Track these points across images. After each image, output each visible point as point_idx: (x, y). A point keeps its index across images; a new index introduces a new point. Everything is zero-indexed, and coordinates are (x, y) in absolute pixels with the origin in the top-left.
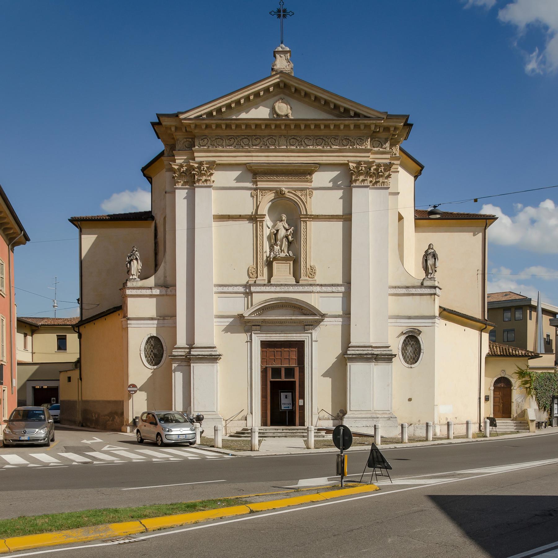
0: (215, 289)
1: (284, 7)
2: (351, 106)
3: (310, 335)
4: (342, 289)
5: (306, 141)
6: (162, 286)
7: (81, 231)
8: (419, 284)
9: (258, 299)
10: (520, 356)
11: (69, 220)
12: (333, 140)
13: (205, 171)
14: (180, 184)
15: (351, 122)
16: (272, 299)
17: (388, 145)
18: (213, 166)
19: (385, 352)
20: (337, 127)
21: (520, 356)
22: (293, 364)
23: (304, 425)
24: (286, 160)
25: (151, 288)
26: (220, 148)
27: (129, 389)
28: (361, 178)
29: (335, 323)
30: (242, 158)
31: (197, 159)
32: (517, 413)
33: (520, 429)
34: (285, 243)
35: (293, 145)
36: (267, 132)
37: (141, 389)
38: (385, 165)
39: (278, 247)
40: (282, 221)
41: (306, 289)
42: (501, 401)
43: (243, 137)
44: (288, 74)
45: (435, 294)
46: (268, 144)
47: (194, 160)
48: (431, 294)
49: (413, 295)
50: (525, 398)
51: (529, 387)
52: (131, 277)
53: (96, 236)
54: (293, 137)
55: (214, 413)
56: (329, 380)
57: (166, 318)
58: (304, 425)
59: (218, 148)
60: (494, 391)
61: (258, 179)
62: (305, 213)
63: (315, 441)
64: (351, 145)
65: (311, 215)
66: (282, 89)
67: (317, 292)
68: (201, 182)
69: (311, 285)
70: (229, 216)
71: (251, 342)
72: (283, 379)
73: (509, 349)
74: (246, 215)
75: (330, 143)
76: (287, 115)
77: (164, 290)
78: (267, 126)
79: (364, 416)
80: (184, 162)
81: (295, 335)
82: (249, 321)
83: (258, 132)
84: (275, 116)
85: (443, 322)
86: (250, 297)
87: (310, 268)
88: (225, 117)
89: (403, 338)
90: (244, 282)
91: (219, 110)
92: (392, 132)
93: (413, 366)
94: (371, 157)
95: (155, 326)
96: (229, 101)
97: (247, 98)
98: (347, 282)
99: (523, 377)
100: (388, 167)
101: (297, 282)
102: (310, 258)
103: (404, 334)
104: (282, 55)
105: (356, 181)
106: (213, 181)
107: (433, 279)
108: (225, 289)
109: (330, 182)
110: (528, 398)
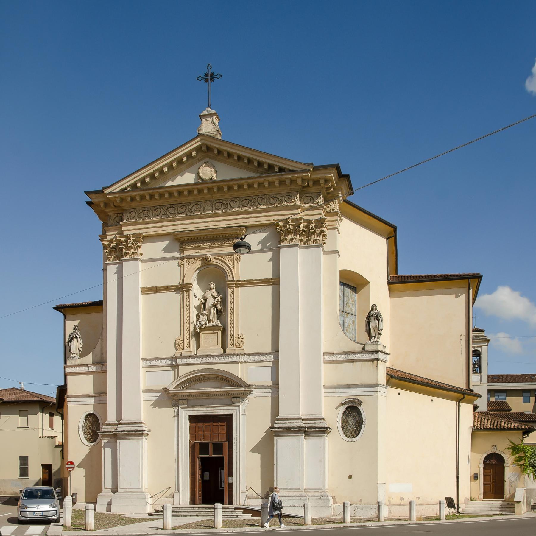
0: (142, 363)
1: (212, 71)
2: (275, 161)
3: (237, 408)
4: (271, 357)
5: (232, 203)
6: (97, 363)
7: (65, 318)
8: (361, 349)
9: (183, 371)
10: (511, 429)
11: (54, 308)
12: (259, 200)
13: (132, 244)
14: (111, 260)
15: (275, 178)
16: (201, 371)
17: (321, 200)
18: (140, 239)
19: (316, 425)
20: (260, 185)
21: (511, 429)
22: (222, 439)
23: (232, 504)
24: (211, 225)
25: (87, 365)
26: (147, 220)
27: (68, 466)
28: (290, 237)
29: (263, 395)
30: (168, 227)
31: (125, 233)
32: (510, 493)
33: (505, 511)
34: (213, 312)
35: (219, 209)
36: (191, 199)
37: (79, 466)
38: (316, 221)
39: (205, 317)
40: (210, 289)
41: (233, 359)
42: (493, 480)
43: (169, 206)
44: (213, 138)
45: (377, 360)
46: (193, 211)
47: (123, 234)
48: (373, 360)
49: (353, 361)
50: (519, 477)
51: (523, 464)
52: (71, 356)
53: (79, 321)
54: (218, 201)
55: (139, 490)
56: (257, 456)
57: (102, 395)
58: (232, 504)
59: (145, 220)
60: (484, 468)
61: (184, 248)
62: (232, 279)
63: (223, 521)
64: (278, 204)
65: (237, 281)
66: (206, 152)
67: (245, 362)
68: (128, 255)
69: (237, 355)
70: (156, 287)
71: (178, 417)
72: (211, 455)
73: (501, 422)
74: (173, 286)
75: (257, 203)
76: (211, 179)
77: (100, 366)
78: (190, 192)
79: (291, 494)
80: (114, 238)
81: (222, 408)
82: (174, 396)
83: (183, 200)
84: (199, 181)
85: (394, 391)
86: (176, 370)
87: (237, 337)
88: (150, 186)
89: (343, 409)
90: (172, 355)
91: (143, 181)
92: (322, 185)
93: (353, 440)
94: (300, 214)
95: (93, 403)
96: (152, 171)
97: (170, 166)
98: (276, 350)
99: (516, 453)
100: (320, 223)
101: (224, 352)
102: (237, 326)
103: (343, 404)
104: (207, 119)
105: (284, 240)
106: (142, 254)
107: (376, 343)
108: (153, 363)
109: (258, 244)
110: (523, 476)
